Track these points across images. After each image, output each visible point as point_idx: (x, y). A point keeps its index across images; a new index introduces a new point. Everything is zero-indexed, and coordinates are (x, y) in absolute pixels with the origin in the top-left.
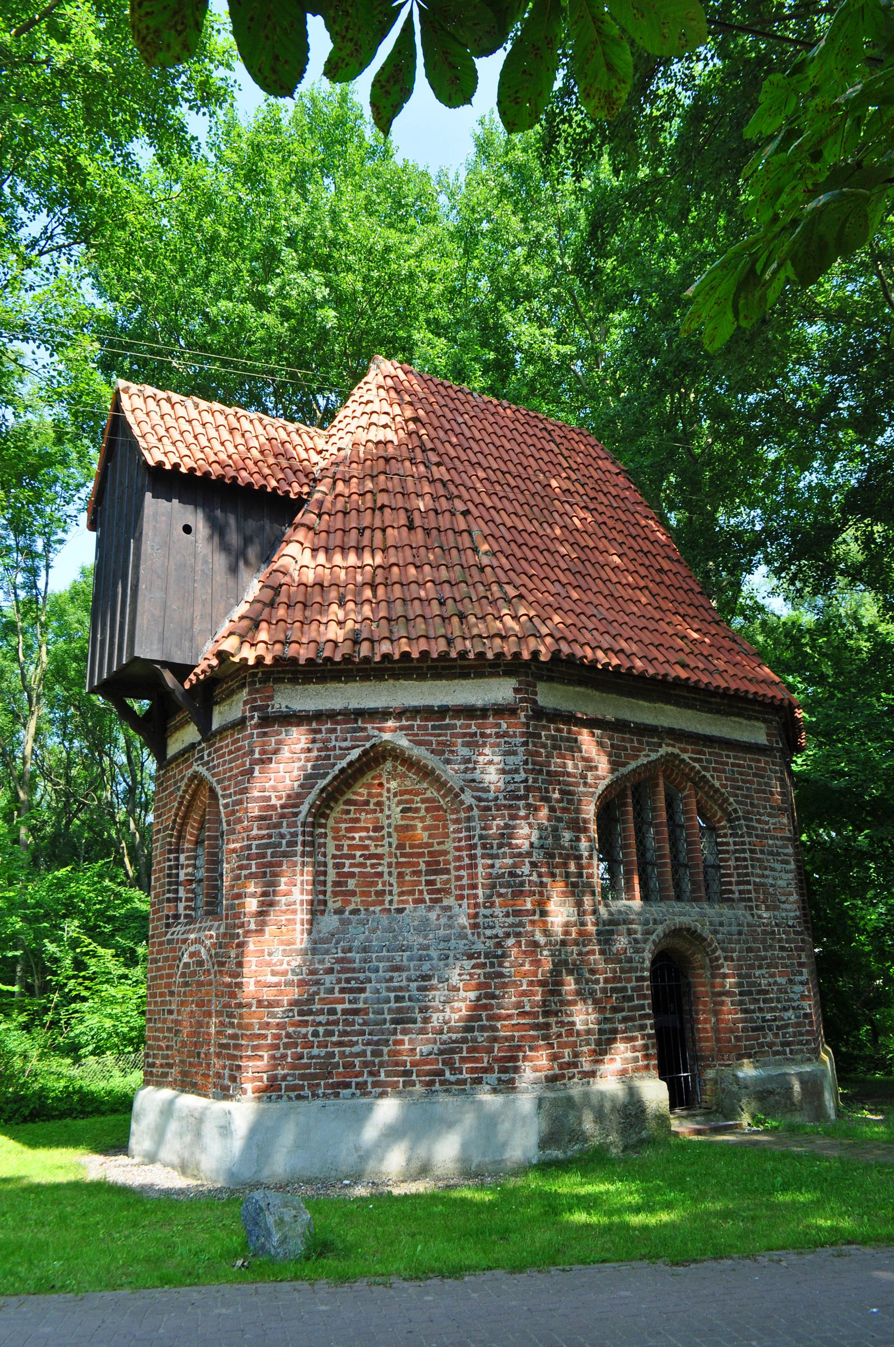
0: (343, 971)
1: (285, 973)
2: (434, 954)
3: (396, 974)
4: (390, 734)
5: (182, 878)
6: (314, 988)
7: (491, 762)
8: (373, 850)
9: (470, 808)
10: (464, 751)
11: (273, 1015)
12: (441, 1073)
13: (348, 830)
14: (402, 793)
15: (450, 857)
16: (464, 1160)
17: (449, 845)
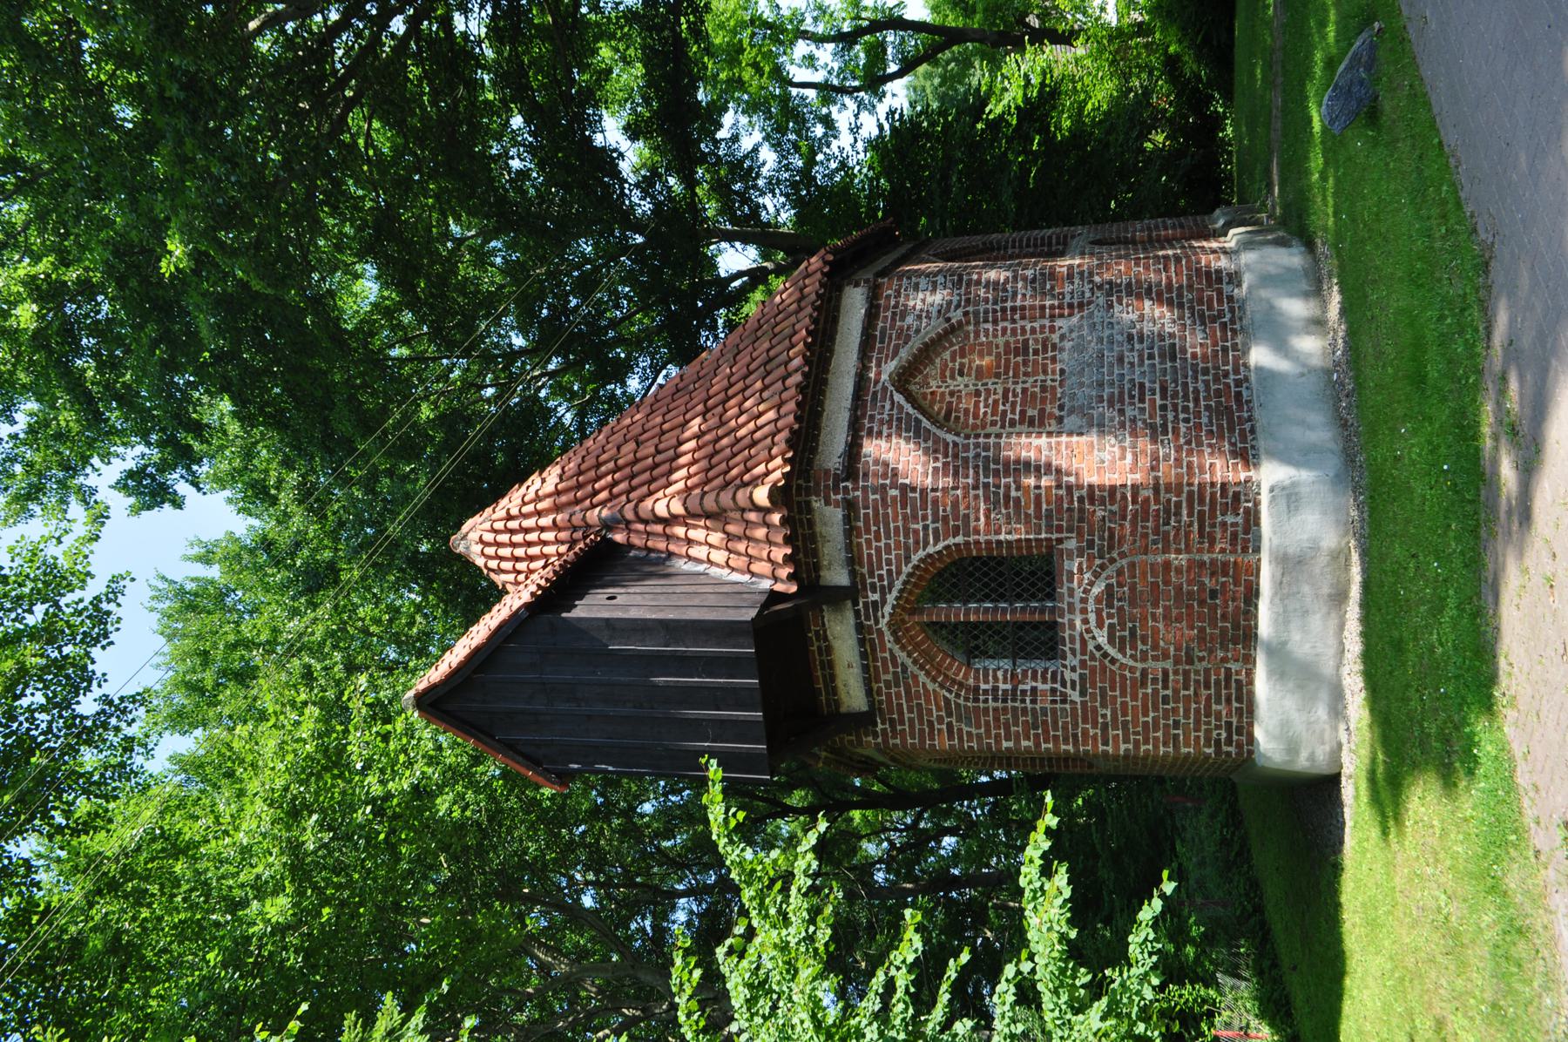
0: (1121, 401)
1: (1123, 449)
2: (1107, 332)
4: (885, 371)
5: (1008, 687)
6: (1140, 424)
7: (923, 301)
8: (999, 396)
9: (966, 314)
10: (910, 320)
11: (1167, 457)
12: (1224, 325)
14: (943, 377)
15: (1012, 340)
16: (1306, 295)
17: (1001, 340)
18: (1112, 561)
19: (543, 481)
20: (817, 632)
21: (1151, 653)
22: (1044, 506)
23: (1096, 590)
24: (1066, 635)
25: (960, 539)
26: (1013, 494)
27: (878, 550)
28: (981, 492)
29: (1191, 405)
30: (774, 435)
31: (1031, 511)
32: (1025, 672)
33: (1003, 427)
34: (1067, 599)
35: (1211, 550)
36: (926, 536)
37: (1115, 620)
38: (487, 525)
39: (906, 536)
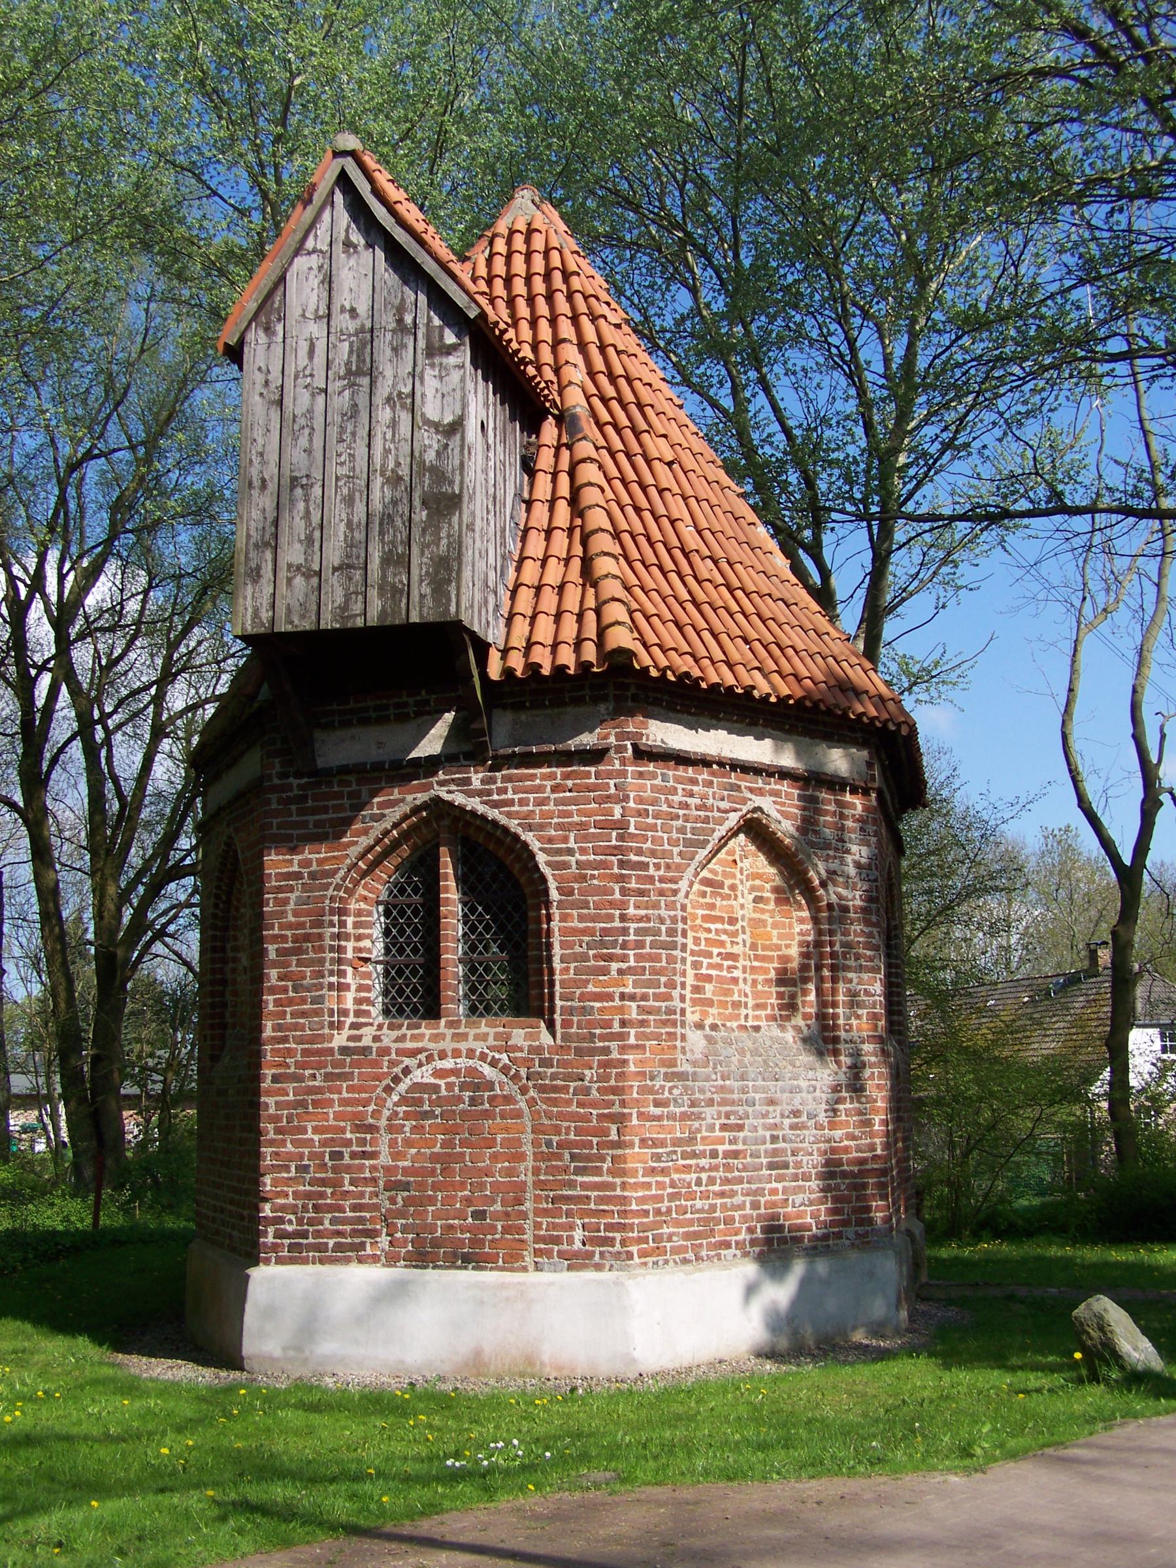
0: (724, 1102)
2: (803, 1084)
3: (771, 1108)
8: (729, 949)
13: (706, 918)
18: (524, 1090)
19: (618, 326)
20: (427, 702)
21: (400, 1137)
22: (597, 1005)
23: (487, 1070)
24: (422, 1030)
25: (554, 895)
26: (615, 966)
27: (540, 789)
28: (617, 924)
29: (717, 1188)
30: (692, 655)
31: (591, 988)
32: (368, 975)
33: (693, 953)
34: (472, 1032)
35: (538, 1212)
36: (559, 852)
37: (444, 1093)
38: (554, 243)
39: (560, 827)
